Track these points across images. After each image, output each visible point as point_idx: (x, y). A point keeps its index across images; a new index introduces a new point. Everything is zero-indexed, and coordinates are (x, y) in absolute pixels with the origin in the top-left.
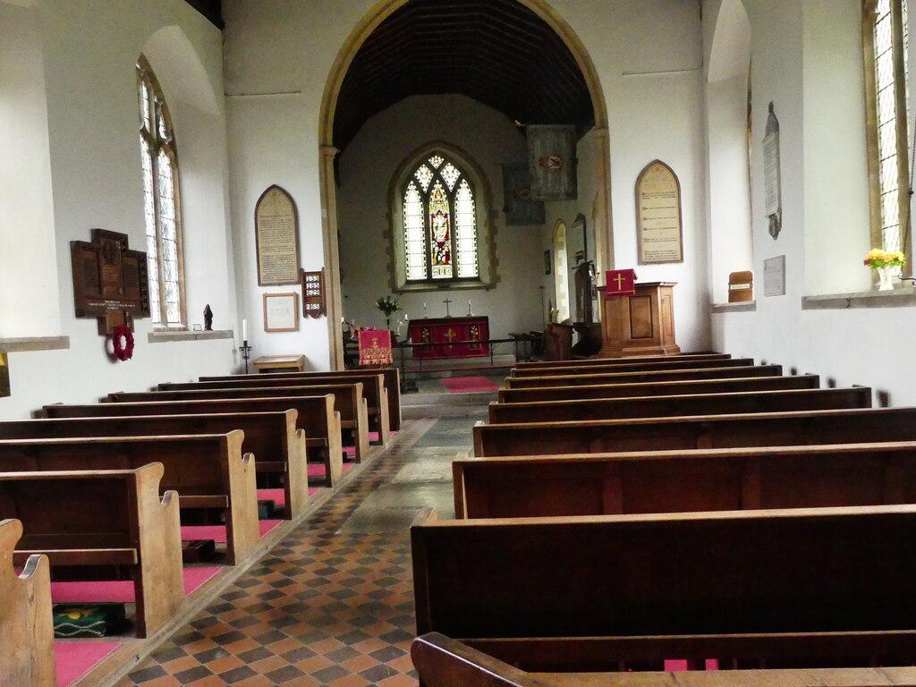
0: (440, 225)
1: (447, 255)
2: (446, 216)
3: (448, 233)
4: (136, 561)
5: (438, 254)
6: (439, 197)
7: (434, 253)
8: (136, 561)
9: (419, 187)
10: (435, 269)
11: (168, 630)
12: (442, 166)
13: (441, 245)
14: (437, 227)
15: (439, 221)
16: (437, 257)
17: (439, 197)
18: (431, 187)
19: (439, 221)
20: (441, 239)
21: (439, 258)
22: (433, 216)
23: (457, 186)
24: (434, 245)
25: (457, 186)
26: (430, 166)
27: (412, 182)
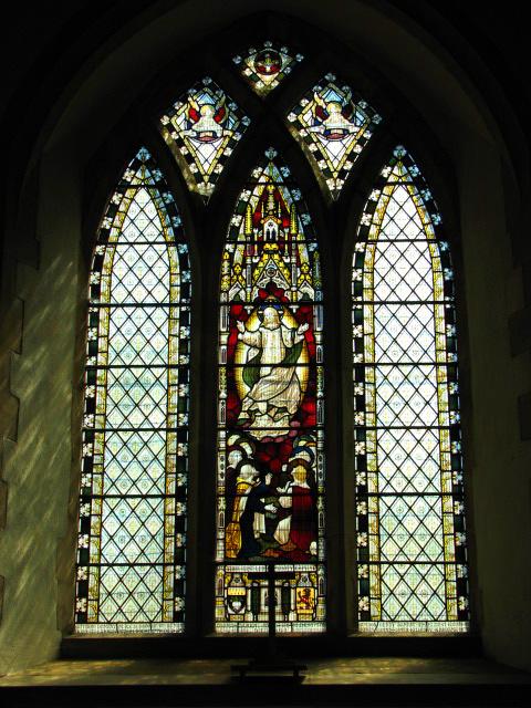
0: (273, 354)
1: (302, 515)
2: (303, 314)
3: (309, 394)
4: (252, 559)
5: (254, 506)
6: (271, 226)
7: (232, 494)
8: (252, 559)
9: (170, 171)
10: (233, 582)
11: (17, 615)
12: (294, 90)
13: (270, 456)
14: (255, 365)
15: (269, 336)
16: (247, 521)
17: (271, 226)
18: (235, 173)
19: (269, 336)
20: (266, 426)
21: (260, 524)
22: (239, 312)
23: (365, 175)
24: (232, 457)
25: (365, 175)
26: (236, 91)
27: (143, 154)
